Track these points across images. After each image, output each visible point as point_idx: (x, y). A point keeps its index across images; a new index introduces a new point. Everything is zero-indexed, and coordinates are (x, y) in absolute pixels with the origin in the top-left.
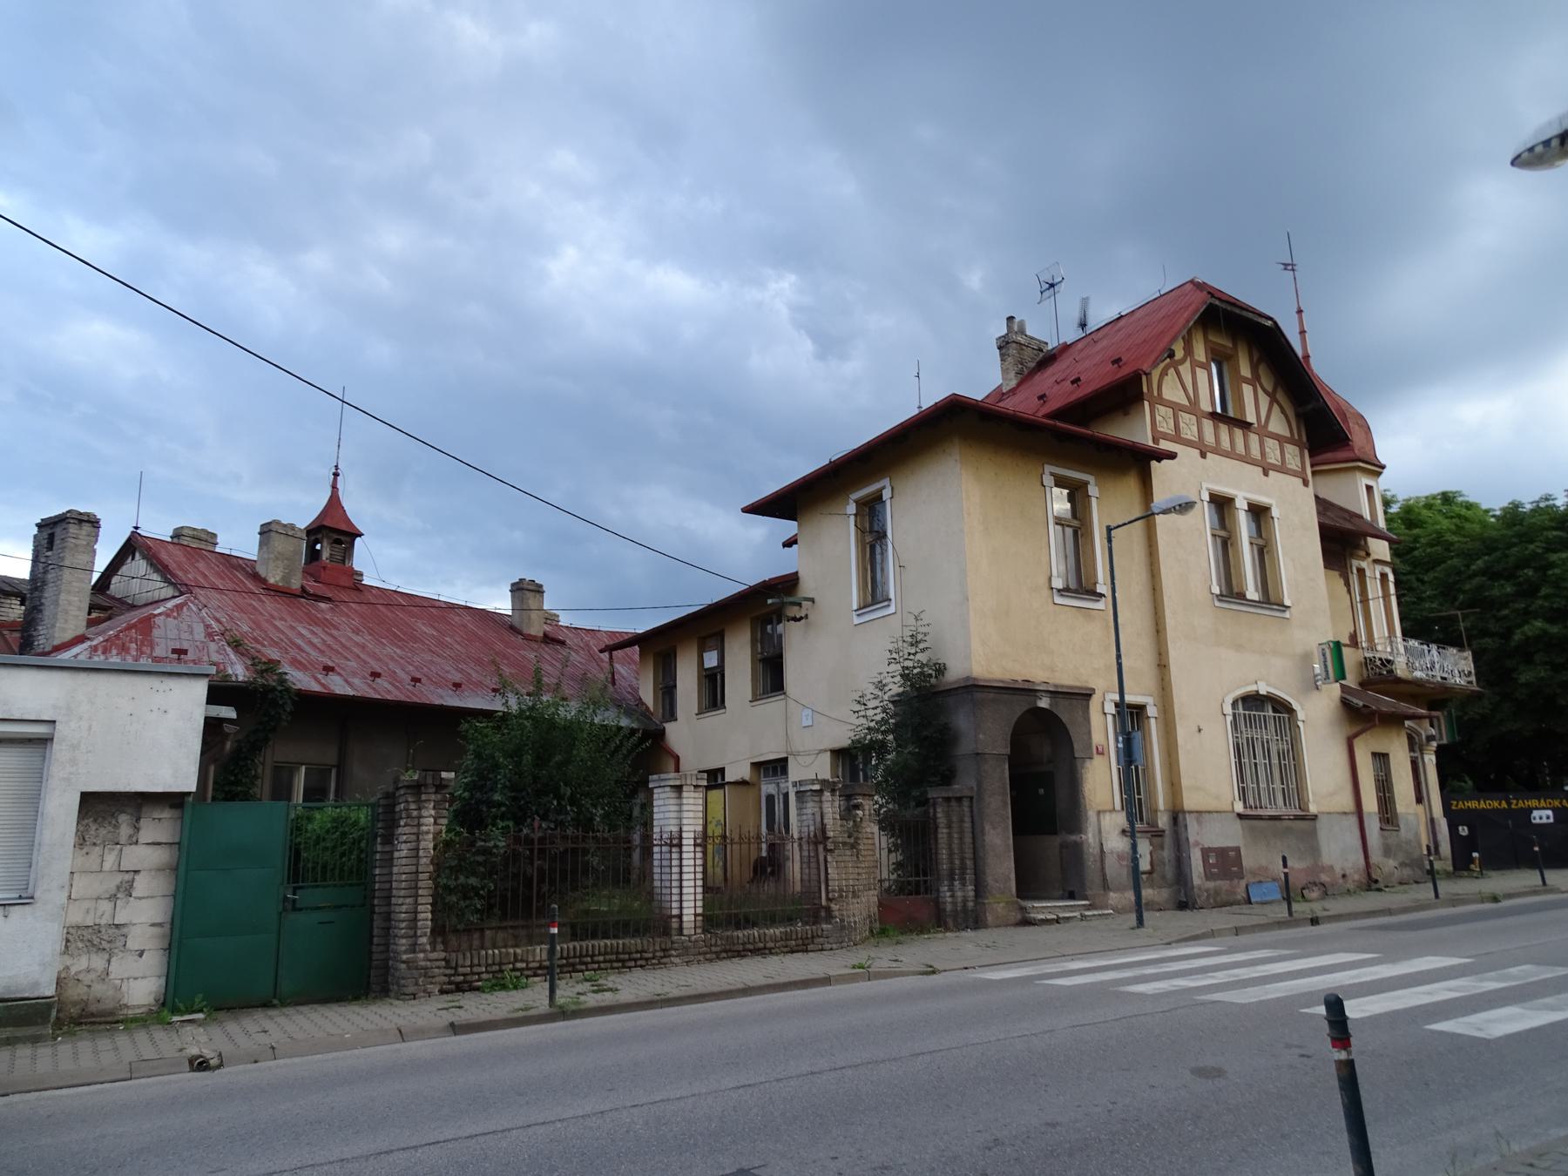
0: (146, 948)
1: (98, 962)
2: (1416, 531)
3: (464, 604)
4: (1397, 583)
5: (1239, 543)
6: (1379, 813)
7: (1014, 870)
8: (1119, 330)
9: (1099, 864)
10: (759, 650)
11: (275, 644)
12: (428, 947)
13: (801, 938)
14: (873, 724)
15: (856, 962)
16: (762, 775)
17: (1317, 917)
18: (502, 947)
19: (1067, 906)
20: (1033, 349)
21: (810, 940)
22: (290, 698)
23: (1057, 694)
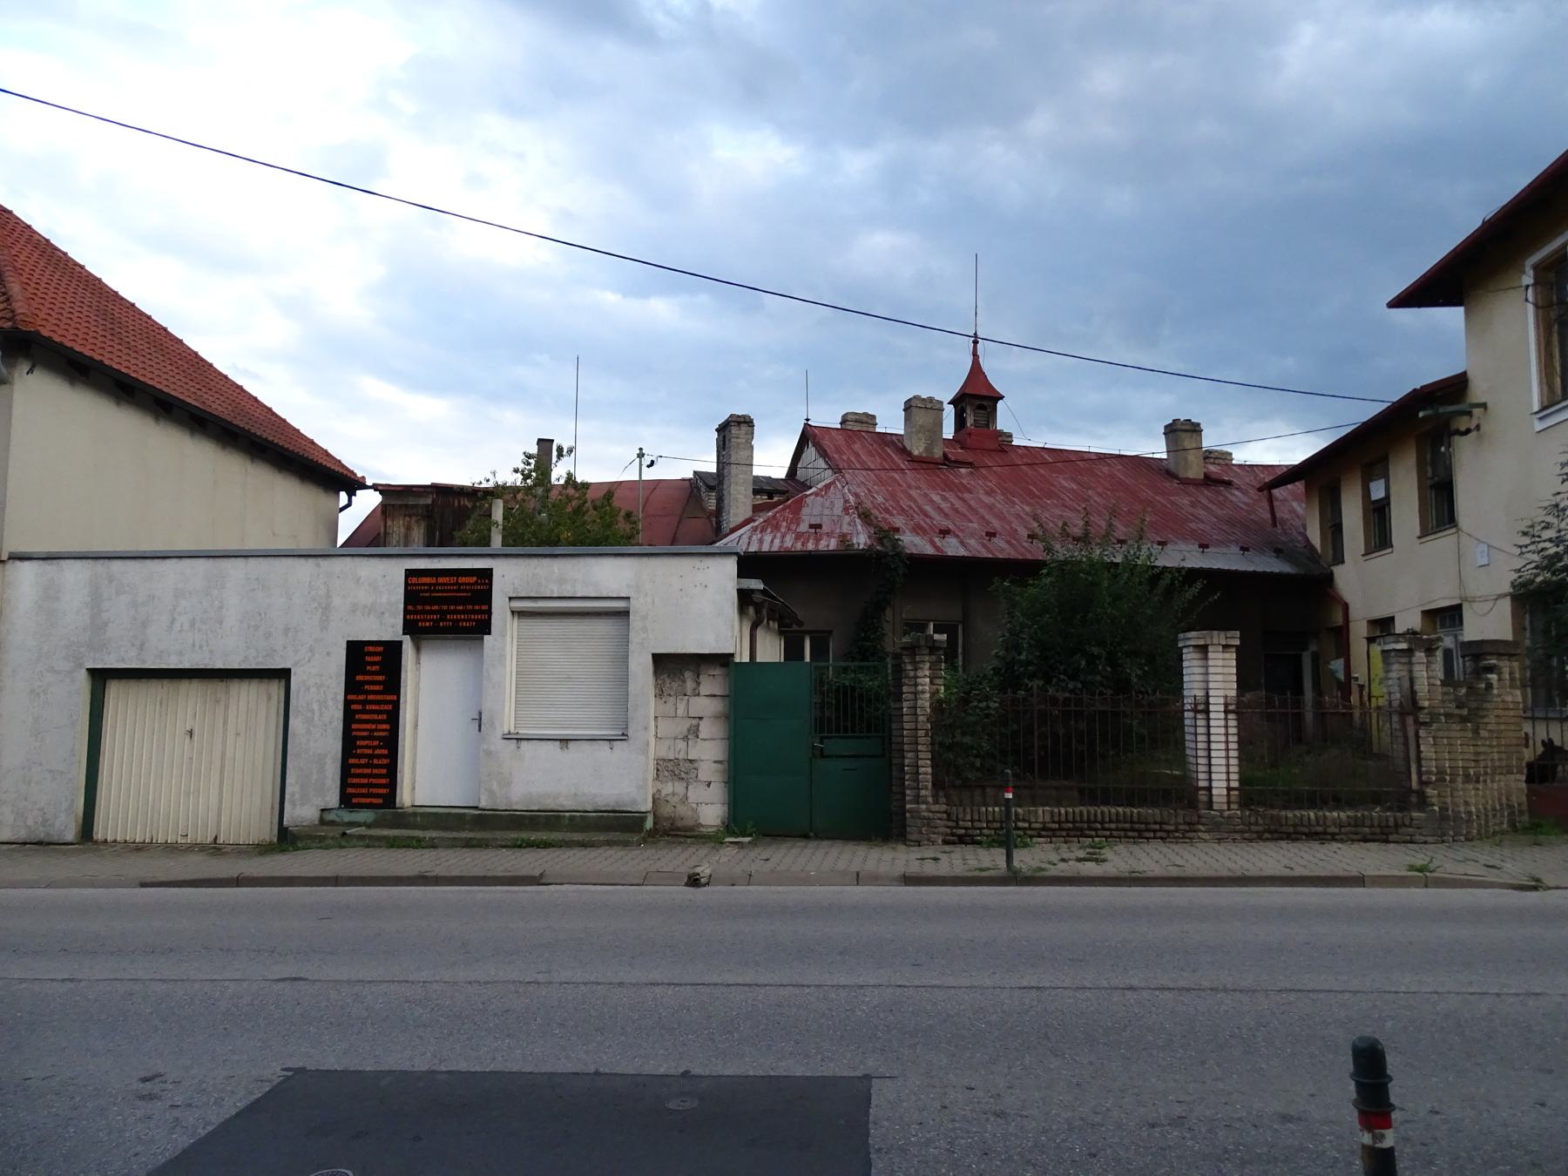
0: (713, 780)
1: (679, 788)
12: (930, 800)
13: (1379, 826)
16: (1438, 626)
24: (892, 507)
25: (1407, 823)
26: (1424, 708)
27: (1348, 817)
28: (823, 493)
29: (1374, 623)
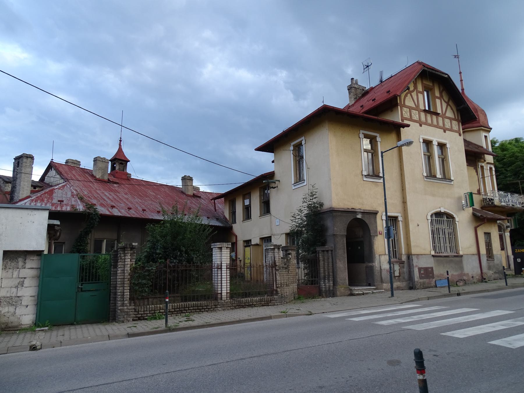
0: (29, 304)
1: (12, 309)
2: (505, 152)
3: (166, 184)
4: (496, 171)
5: (434, 158)
6: (487, 254)
7: (347, 276)
8: (391, 81)
9: (380, 274)
10: (262, 198)
11: (95, 198)
12: (128, 305)
13: (266, 301)
14: (297, 224)
15: (282, 310)
17: (460, 293)
18: (156, 305)
19: (367, 289)
20: (361, 90)
21: (270, 302)
22: (98, 217)
23: (364, 213)
24: (91, 196)
25: (273, 299)
26: (277, 265)
27: (259, 299)
28: (62, 189)
29: (245, 241)
